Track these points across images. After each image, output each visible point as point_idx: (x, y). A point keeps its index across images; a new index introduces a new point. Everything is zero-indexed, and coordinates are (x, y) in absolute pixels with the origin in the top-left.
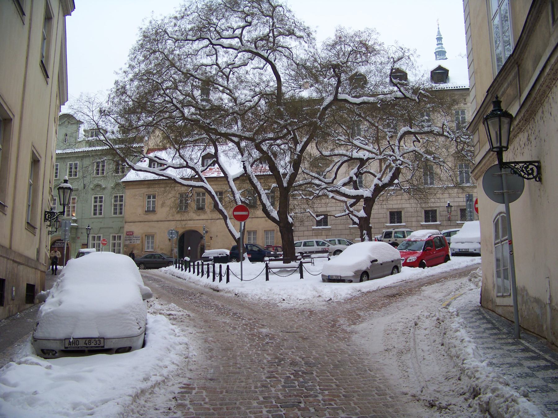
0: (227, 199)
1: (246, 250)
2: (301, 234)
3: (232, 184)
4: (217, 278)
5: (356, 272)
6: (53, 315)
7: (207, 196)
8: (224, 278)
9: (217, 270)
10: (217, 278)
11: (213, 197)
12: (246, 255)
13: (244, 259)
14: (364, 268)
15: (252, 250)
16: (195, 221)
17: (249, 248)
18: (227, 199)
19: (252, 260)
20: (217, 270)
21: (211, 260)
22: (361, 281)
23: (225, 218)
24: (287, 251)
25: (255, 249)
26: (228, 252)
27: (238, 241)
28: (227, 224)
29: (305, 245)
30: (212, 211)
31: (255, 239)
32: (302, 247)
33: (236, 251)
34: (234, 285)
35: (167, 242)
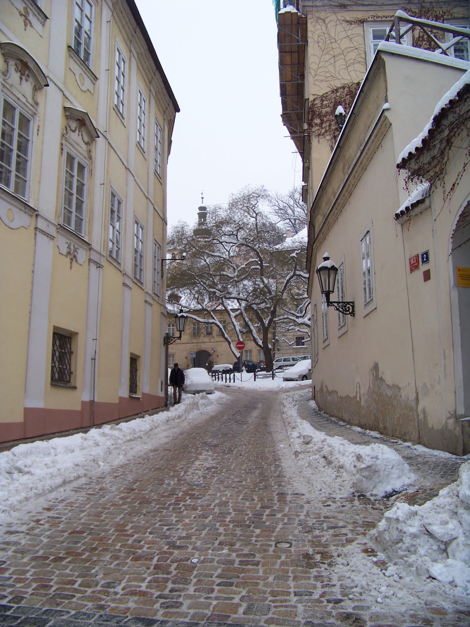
0: (229, 328)
1: (244, 365)
2: (285, 351)
3: (234, 320)
4: (228, 381)
5: (300, 376)
6: (190, 385)
7: (215, 328)
8: (232, 381)
9: (228, 378)
10: (228, 381)
11: (218, 326)
12: (244, 368)
13: (242, 371)
14: (304, 374)
15: (248, 365)
16: (206, 344)
17: (246, 363)
18: (229, 328)
19: (248, 372)
20: (228, 378)
21: (220, 372)
22: (303, 380)
23: (229, 343)
24: (268, 366)
25: (250, 364)
26: (231, 367)
27: (238, 359)
28: (230, 348)
29: (285, 360)
30: (218, 335)
31: (250, 356)
32: (282, 362)
33: (237, 366)
34: (238, 383)
35: (184, 359)
